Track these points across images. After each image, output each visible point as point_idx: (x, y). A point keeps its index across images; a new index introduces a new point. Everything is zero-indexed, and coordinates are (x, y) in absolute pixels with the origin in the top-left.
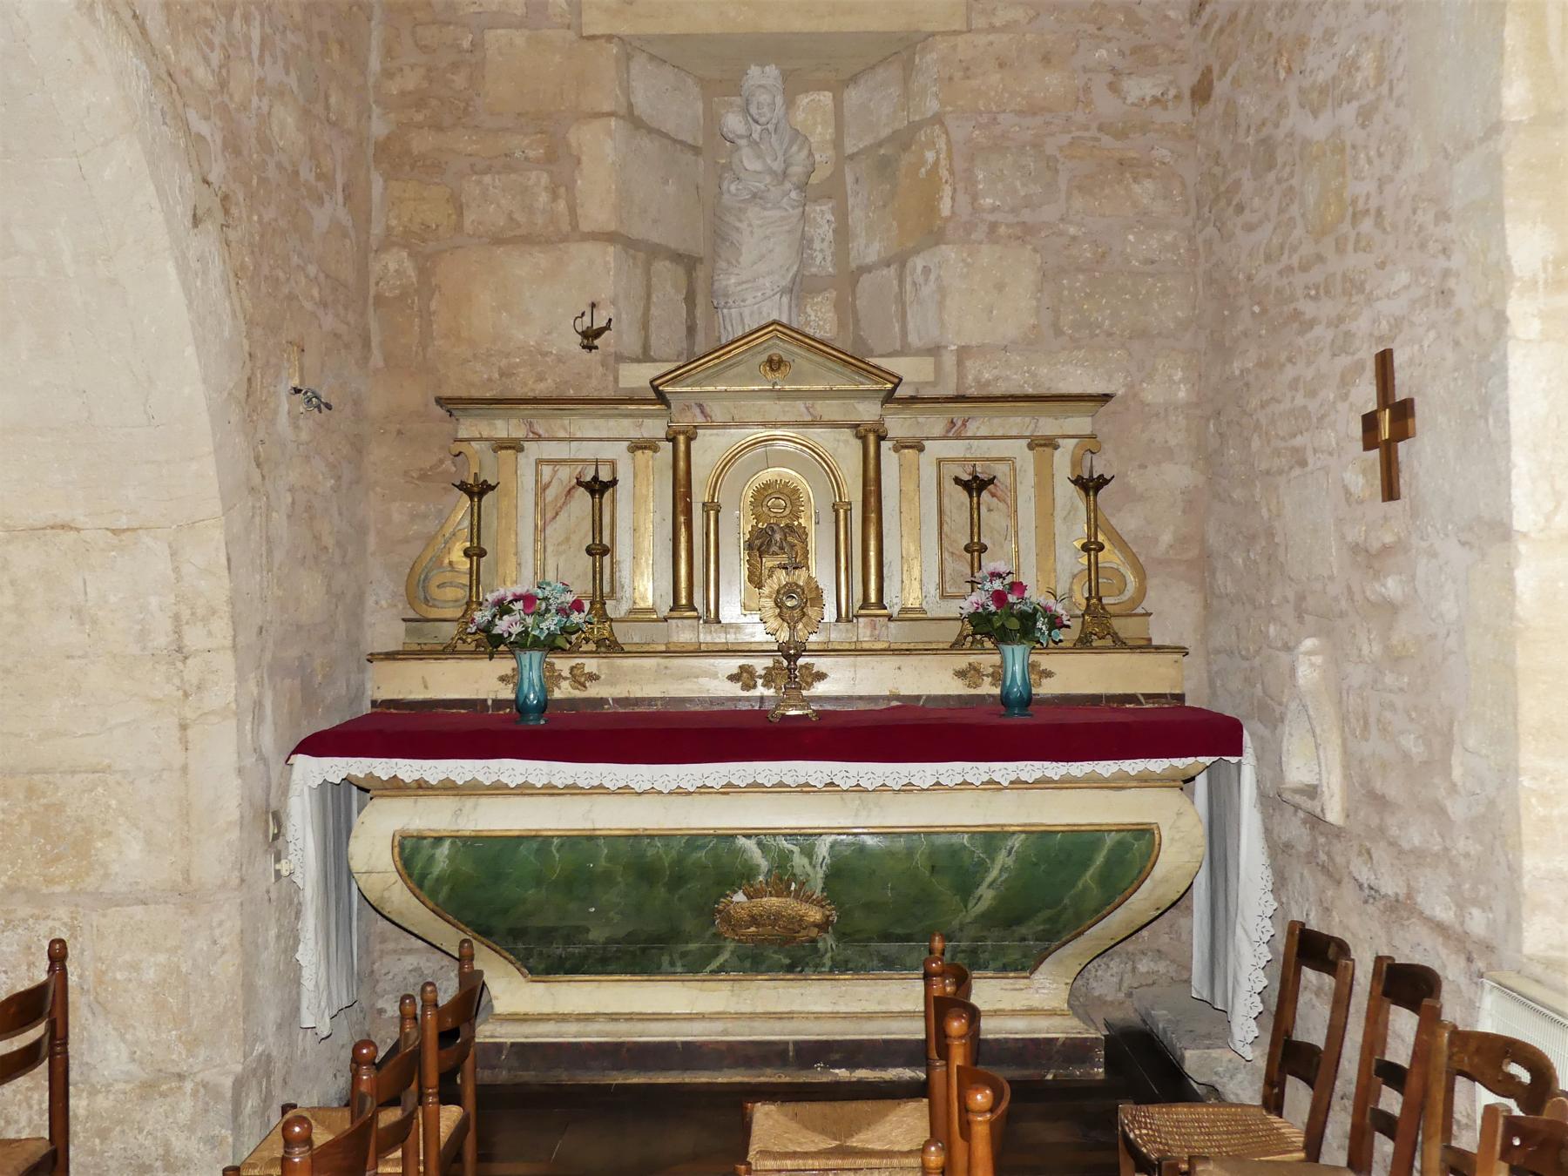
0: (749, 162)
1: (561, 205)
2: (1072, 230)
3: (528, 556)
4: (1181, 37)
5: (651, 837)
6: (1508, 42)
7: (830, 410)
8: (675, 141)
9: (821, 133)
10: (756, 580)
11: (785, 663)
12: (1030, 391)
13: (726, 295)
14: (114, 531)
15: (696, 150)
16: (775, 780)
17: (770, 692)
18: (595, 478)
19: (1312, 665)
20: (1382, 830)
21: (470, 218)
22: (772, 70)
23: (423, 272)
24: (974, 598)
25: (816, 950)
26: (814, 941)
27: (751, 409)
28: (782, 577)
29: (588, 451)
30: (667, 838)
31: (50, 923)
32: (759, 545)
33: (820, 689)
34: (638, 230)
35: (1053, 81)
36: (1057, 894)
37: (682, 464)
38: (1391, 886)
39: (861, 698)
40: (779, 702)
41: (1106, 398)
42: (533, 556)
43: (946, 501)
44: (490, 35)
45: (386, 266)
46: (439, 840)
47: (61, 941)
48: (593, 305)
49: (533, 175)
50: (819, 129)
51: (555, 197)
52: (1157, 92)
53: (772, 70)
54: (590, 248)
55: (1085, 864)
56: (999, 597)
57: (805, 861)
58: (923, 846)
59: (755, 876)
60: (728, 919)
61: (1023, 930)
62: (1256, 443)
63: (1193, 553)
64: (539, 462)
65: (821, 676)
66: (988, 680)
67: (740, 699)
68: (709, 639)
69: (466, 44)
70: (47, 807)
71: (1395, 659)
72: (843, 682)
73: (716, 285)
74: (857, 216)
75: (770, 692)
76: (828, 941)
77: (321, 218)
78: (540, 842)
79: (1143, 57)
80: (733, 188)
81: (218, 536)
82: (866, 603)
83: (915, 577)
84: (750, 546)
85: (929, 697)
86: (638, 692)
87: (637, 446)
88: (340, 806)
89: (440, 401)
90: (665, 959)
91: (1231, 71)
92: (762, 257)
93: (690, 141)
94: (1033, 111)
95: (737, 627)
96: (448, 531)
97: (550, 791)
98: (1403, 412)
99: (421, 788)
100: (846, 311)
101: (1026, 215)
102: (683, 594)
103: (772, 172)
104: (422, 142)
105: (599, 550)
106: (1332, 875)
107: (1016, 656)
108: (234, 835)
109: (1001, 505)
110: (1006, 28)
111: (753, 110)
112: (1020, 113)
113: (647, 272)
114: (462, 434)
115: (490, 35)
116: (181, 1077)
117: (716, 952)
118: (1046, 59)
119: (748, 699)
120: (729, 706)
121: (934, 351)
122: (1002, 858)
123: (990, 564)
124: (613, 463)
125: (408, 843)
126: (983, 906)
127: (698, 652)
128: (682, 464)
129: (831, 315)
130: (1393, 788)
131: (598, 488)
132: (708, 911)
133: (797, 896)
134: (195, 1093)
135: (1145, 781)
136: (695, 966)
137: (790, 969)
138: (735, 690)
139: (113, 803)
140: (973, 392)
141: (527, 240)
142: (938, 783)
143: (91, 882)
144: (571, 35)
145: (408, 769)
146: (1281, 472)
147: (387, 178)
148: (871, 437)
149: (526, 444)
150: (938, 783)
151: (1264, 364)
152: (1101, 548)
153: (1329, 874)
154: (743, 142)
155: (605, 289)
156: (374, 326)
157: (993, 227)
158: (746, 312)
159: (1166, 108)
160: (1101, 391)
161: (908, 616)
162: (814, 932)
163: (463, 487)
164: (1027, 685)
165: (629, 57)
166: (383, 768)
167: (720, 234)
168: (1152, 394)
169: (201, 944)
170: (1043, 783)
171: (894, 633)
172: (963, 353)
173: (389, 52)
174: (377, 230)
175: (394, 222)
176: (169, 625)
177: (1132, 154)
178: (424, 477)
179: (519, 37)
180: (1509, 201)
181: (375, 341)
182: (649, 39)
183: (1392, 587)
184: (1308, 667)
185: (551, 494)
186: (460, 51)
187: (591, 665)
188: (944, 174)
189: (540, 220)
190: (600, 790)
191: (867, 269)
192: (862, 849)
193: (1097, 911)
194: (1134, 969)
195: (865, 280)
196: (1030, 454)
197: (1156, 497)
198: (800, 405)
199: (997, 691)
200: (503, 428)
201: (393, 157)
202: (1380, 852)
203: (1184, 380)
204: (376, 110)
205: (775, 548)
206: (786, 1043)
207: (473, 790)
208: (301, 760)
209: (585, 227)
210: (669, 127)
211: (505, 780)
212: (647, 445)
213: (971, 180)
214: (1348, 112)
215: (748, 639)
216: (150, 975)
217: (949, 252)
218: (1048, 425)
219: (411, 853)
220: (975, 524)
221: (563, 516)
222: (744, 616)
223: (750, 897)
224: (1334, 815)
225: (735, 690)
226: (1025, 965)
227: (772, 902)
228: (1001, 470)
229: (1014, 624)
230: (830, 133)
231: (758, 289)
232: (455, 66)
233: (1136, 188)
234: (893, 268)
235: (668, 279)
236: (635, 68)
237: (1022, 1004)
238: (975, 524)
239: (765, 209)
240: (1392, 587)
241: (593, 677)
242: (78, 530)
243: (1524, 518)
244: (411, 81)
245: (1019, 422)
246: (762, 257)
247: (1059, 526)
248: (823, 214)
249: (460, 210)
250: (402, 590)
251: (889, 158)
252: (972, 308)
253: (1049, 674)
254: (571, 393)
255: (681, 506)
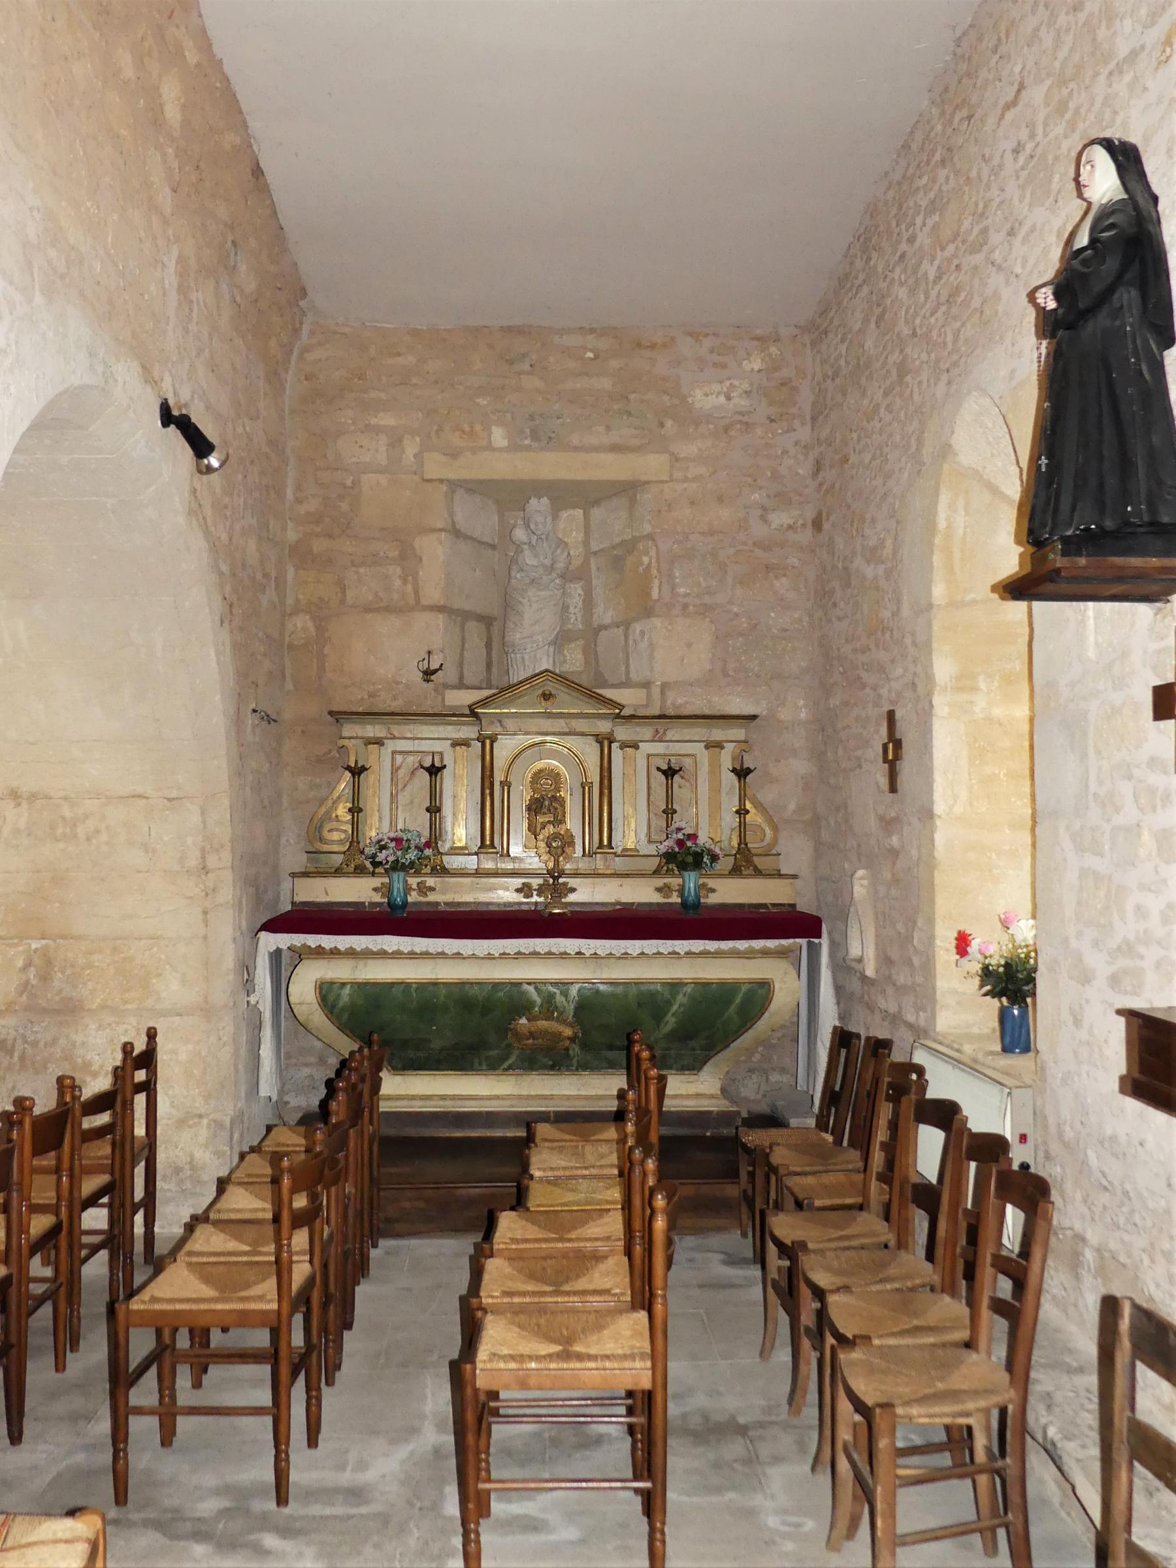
0: (529, 559)
1: (409, 588)
2: (735, 609)
3: (386, 813)
4: (807, 487)
5: (472, 983)
6: (935, 564)
7: (581, 725)
8: (479, 542)
9: (575, 537)
10: (533, 830)
11: (551, 881)
12: (707, 712)
13: (513, 645)
14: (169, 799)
15: (493, 547)
16: (546, 950)
17: (541, 899)
18: (433, 765)
19: (862, 885)
20: (890, 977)
21: (350, 595)
22: (545, 501)
23: (318, 628)
24: (666, 843)
25: (568, 1055)
26: (567, 1049)
27: (533, 724)
28: (550, 829)
29: (426, 746)
30: (480, 984)
31: (125, 1026)
32: (535, 808)
33: (572, 898)
34: (459, 603)
35: (725, 514)
36: (711, 1023)
37: (488, 757)
38: (892, 1009)
39: (597, 904)
40: (547, 905)
41: (754, 717)
42: (390, 814)
43: (652, 780)
44: (364, 477)
45: (295, 625)
46: (344, 984)
47: (155, 1029)
48: (429, 652)
49: (391, 568)
50: (574, 534)
51: (405, 581)
52: (791, 522)
53: (545, 501)
54: (427, 616)
55: (729, 1002)
56: (680, 843)
57: (563, 999)
58: (633, 991)
59: (533, 1007)
60: (516, 1034)
61: (693, 1044)
62: (840, 752)
63: (807, 817)
64: (394, 753)
65: (573, 890)
66: (675, 894)
67: (523, 903)
68: (503, 866)
69: (349, 483)
70: (124, 959)
71: (896, 881)
72: (586, 893)
73: (507, 639)
74: (599, 593)
75: (541, 899)
76: (575, 1050)
77: (264, 601)
78: (405, 986)
79: (782, 499)
80: (518, 576)
81: (226, 802)
82: (601, 846)
83: (633, 829)
84: (529, 809)
85: (639, 904)
86: (458, 899)
87: (456, 744)
88: (282, 968)
89: (331, 713)
90: (476, 1060)
91: (831, 518)
92: (536, 622)
93: (490, 542)
94: (712, 533)
95: (520, 859)
96: (336, 794)
97: (412, 955)
98: (898, 744)
99: (335, 953)
100: (590, 653)
101: (707, 600)
102: (488, 838)
103: (544, 566)
104: (319, 546)
105: (434, 810)
106: (871, 1007)
107: (691, 880)
108: (231, 977)
109: (688, 785)
110: (695, 479)
111: (532, 526)
112: (703, 534)
113: (463, 631)
114: (346, 733)
115: (364, 477)
116: (201, 1116)
117: (507, 1059)
118: (720, 500)
119: (527, 903)
120: (516, 908)
121: (646, 685)
122: (680, 999)
123: (677, 822)
124: (441, 754)
125: (325, 987)
126: (668, 1028)
127: (496, 874)
128: (488, 757)
129: (580, 656)
130: (895, 955)
131: (434, 771)
132: (504, 1028)
133: (558, 1020)
134: (209, 1126)
135: (765, 953)
136: (494, 1066)
137: (552, 1068)
138: (520, 898)
139: (163, 957)
140: (671, 712)
141: (389, 609)
142: (643, 953)
143: (150, 1003)
144: (417, 478)
145: (327, 941)
146: (851, 770)
147: (297, 568)
148: (605, 741)
149: (386, 741)
150: (643, 953)
151: (846, 704)
152: (748, 812)
153: (869, 1008)
154: (525, 547)
155: (437, 642)
156: (288, 664)
157: (685, 607)
158: (526, 657)
159: (796, 532)
160: (752, 713)
161: (626, 853)
162: (567, 1043)
163: (348, 768)
164: (698, 897)
165: (454, 492)
166: (313, 940)
167: (508, 604)
168: (784, 714)
169: (213, 1039)
170: (704, 954)
171: (619, 864)
172: (664, 687)
173: (299, 488)
174: (290, 601)
175: (301, 597)
176: (198, 854)
177: (775, 561)
178: (319, 760)
179: (383, 479)
180: (935, 645)
181: (288, 675)
182: (465, 481)
183: (895, 841)
184: (860, 887)
185: (401, 773)
186: (344, 486)
187: (430, 882)
188: (654, 572)
189: (396, 596)
190: (442, 955)
191: (605, 627)
192: (598, 991)
193: (737, 1032)
194: (767, 1079)
195: (603, 633)
196: (706, 752)
197: (786, 778)
198: (562, 722)
199: (679, 900)
200: (372, 730)
201: (301, 555)
202: (890, 991)
203: (805, 706)
204: (290, 525)
205: (545, 810)
206: (549, 1112)
207: (367, 954)
208: (263, 935)
209: (425, 601)
210: (476, 534)
211: (386, 948)
212: (465, 743)
213: (671, 576)
214: (881, 569)
215: (528, 867)
216: (183, 1057)
217: (657, 622)
218: (717, 734)
219: (326, 993)
220: (669, 798)
221: (409, 787)
222: (523, 851)
223: (529, 1020)
224: (870, 972)
225: (520, 898)
226: (694, 1066)
227: (543, 1024)
228: (687, 762)
229: (690, 859)
230: (581, 536)
231: (534, 642)
232: (341, 497)
233: (776, 583)
234: (621, 628)
235: (475, 633)
236: (457, 498)
237: (691, 1091)
238: (669, 798)
239: (539, 590)
240: (895, 841)
241: (432, 889)
242: (147, 798)
243: (939, 808)
244: (313, 505)
245: (699, 732)
246: (536, 622)
247: (724, 798)
248: (576, 590)
249: (343, 590)
250: (303, 833)
251: (619, 557)
252: (671, 657)
253: (713, 891)
254: (414, 709)
255: (487, 784)
